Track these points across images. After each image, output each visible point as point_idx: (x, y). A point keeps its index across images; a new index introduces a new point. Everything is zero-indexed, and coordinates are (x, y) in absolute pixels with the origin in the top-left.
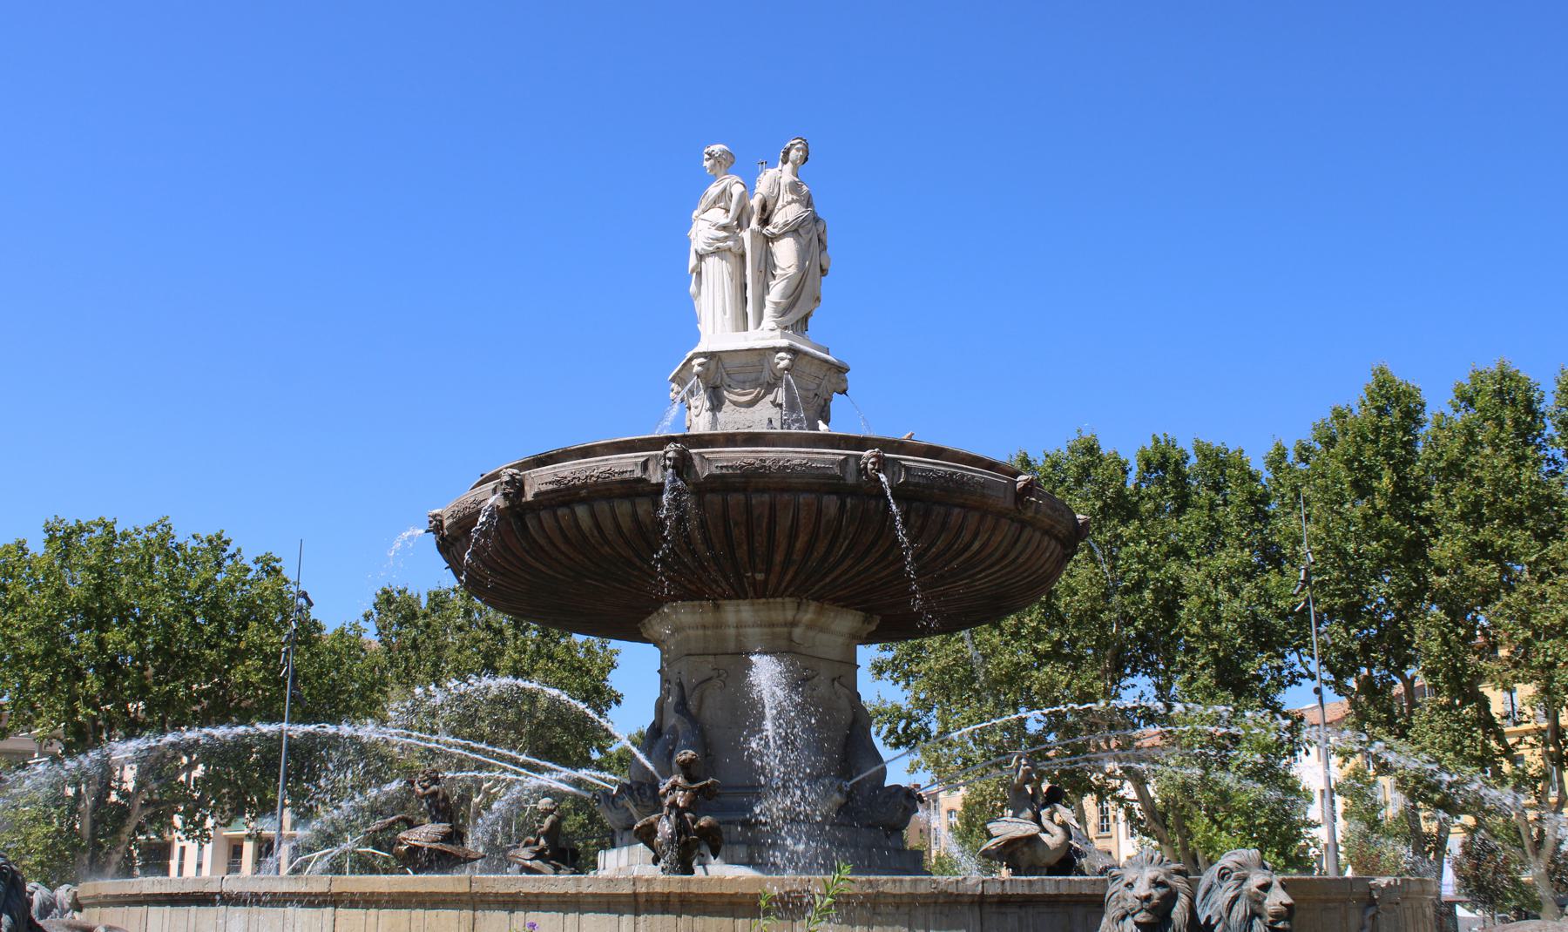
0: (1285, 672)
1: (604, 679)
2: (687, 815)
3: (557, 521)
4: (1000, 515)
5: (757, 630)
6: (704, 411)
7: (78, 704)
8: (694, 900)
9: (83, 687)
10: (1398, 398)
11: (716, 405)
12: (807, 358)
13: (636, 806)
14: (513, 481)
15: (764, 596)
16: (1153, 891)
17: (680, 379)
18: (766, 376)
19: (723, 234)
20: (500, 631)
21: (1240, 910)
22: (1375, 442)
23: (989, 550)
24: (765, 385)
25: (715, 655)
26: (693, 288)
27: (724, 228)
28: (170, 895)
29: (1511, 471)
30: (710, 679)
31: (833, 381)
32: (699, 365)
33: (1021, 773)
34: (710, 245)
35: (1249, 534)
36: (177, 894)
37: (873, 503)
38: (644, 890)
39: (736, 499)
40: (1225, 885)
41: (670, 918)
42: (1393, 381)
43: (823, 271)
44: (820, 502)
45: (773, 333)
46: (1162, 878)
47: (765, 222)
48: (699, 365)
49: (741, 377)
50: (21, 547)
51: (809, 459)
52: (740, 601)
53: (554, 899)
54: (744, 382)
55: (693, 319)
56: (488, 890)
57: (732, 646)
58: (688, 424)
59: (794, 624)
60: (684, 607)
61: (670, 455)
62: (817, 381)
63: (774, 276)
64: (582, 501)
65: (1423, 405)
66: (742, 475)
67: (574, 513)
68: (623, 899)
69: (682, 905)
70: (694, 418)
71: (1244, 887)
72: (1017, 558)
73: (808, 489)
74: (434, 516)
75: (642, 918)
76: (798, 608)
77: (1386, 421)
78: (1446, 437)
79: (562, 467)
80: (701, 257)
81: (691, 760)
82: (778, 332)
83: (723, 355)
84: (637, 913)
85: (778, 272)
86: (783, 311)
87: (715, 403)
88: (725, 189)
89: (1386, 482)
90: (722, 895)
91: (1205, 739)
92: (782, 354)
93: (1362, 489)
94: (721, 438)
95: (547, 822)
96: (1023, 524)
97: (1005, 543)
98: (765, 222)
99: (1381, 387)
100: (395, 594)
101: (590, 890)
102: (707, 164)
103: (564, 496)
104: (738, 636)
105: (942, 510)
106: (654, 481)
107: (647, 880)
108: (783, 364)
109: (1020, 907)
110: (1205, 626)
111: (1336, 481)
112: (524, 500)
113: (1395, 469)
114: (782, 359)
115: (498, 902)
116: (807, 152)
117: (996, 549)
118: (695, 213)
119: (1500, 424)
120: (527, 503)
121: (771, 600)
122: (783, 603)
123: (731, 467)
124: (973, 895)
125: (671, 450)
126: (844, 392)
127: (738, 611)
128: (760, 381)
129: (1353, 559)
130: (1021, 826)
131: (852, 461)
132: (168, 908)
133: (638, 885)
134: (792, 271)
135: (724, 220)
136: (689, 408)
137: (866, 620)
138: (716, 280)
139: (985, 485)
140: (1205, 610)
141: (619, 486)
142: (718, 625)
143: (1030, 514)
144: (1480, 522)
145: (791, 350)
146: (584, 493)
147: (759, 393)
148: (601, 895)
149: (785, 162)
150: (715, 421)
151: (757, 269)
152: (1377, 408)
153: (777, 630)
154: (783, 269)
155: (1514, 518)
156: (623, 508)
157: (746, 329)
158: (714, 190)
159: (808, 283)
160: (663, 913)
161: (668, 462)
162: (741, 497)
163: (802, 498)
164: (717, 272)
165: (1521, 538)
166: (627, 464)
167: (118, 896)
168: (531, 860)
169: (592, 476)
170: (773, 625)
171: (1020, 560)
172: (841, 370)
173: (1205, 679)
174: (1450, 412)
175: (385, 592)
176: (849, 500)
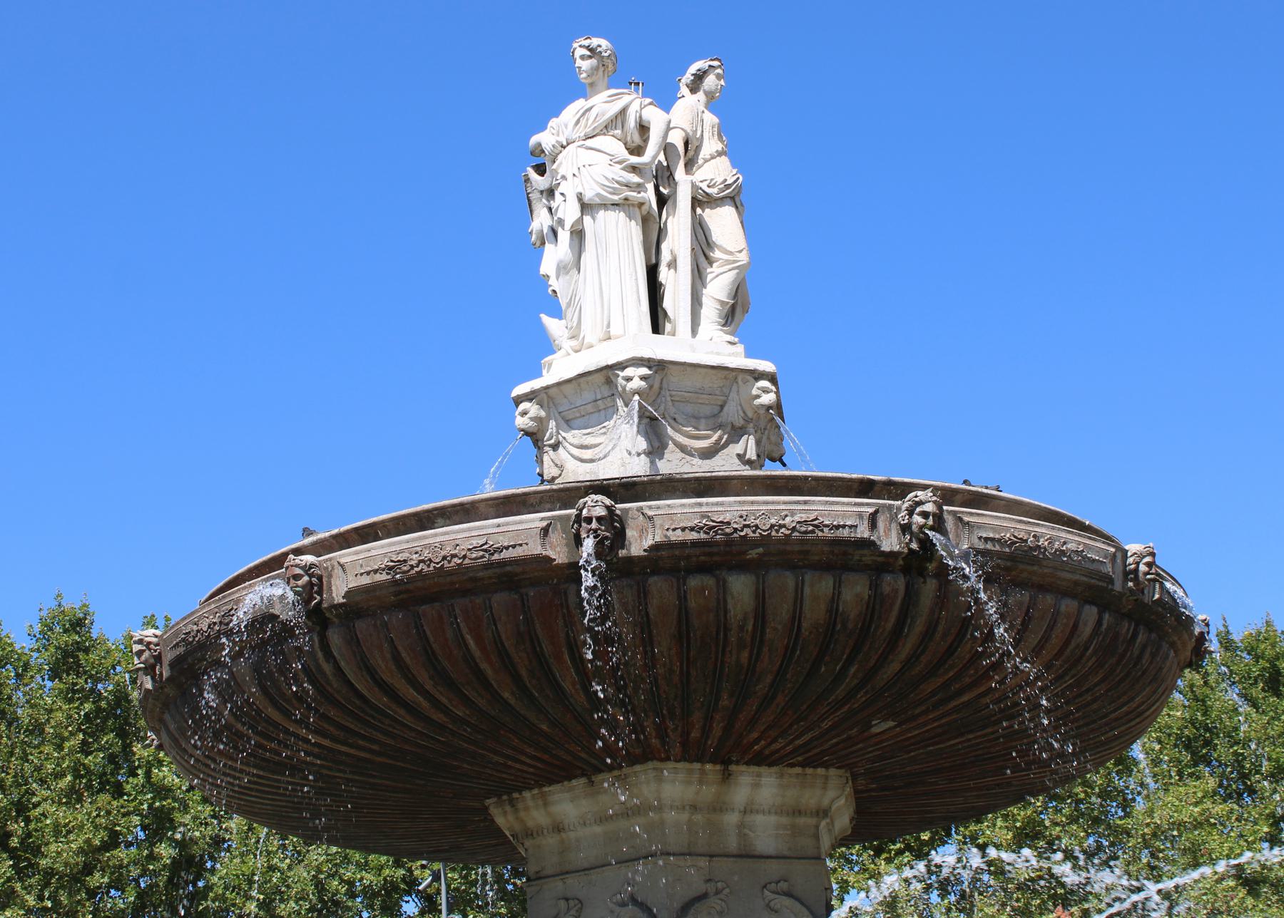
3: (683, 598)
5: (773, 819)
18: (732, 413)
24: (729, 428)
25: (712, 856)
30: (703, 897)
32: (643, 378)
44: (1079, 612)
45: (732, 349)
48: (643, 378)
49: (689, 408)
54: (697, 418)
57: (732, 844)
60: (676, 770)
64: (743, 566)
67: (723, 586)
76: (546, 804)
79: (717, 504)
87: (656, 444)
92: (764, 383)
102: (585, 65)
104: (741, 826)
112: (622, 553)
114: (766, 391)
120: (630, 560)
121: (809, 771)
122: (826, 778)
123: (999, 541)
127: (756, 786)
141: (826, 549)
146: (753, 553)
147: (720, 438)
153: (801, 821)
154: (731, 253)
156: (819, 587)
161: (918, 519)
162: (709, 581)
163: (1068, 605)
169: (781, 526)
170: (800, 812)
174: (112, 640)
176: (1107, 616)
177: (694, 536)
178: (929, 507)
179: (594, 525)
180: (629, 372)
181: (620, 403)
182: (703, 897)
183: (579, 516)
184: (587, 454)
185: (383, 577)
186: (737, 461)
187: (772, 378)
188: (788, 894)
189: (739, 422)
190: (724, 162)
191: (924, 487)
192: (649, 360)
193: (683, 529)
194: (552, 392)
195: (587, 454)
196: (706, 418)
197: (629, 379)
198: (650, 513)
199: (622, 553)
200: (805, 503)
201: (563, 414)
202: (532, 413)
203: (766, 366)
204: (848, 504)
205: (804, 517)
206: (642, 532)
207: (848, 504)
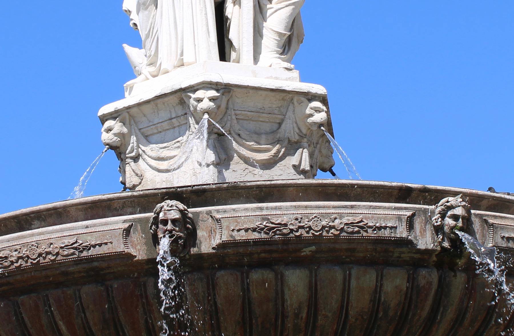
3: (246, 290)
24: (286, 142)
32: (212, 99)
48: (212, 99)
49: (252, 126)
54: (259, 134)
67: (281, 279)
79: (276, 208)
87: (223, 157)
120: (200, 256)
141: (370, 247)
146: (307, 251)
147: (279, 151)
161: (449, 222)
162: (268, 275)
169: (331, 227)
177: (256, 236)
178: (459, 211)
179: (170, 226)
180: (200, 94)
181: (192, 121)
183: (156, 218)
184: (163, 165)
186: (293, 171)
187: (324, 100)
189: (295, 138)
191: (455, 194)
192: (217, 84)
193: (247, 230)
194: (133, 111)
195: (163, 165)
196: (267, 133)
197: (199, 100)
198: (218, 216)
199: (194, 250)
200: (352, 207)
201: (142, 130)
202: (116, 130)
203: (318, 89)
204: (389, 208)
205: (351, 219)
206: (211, 232)
207: (389, 208)
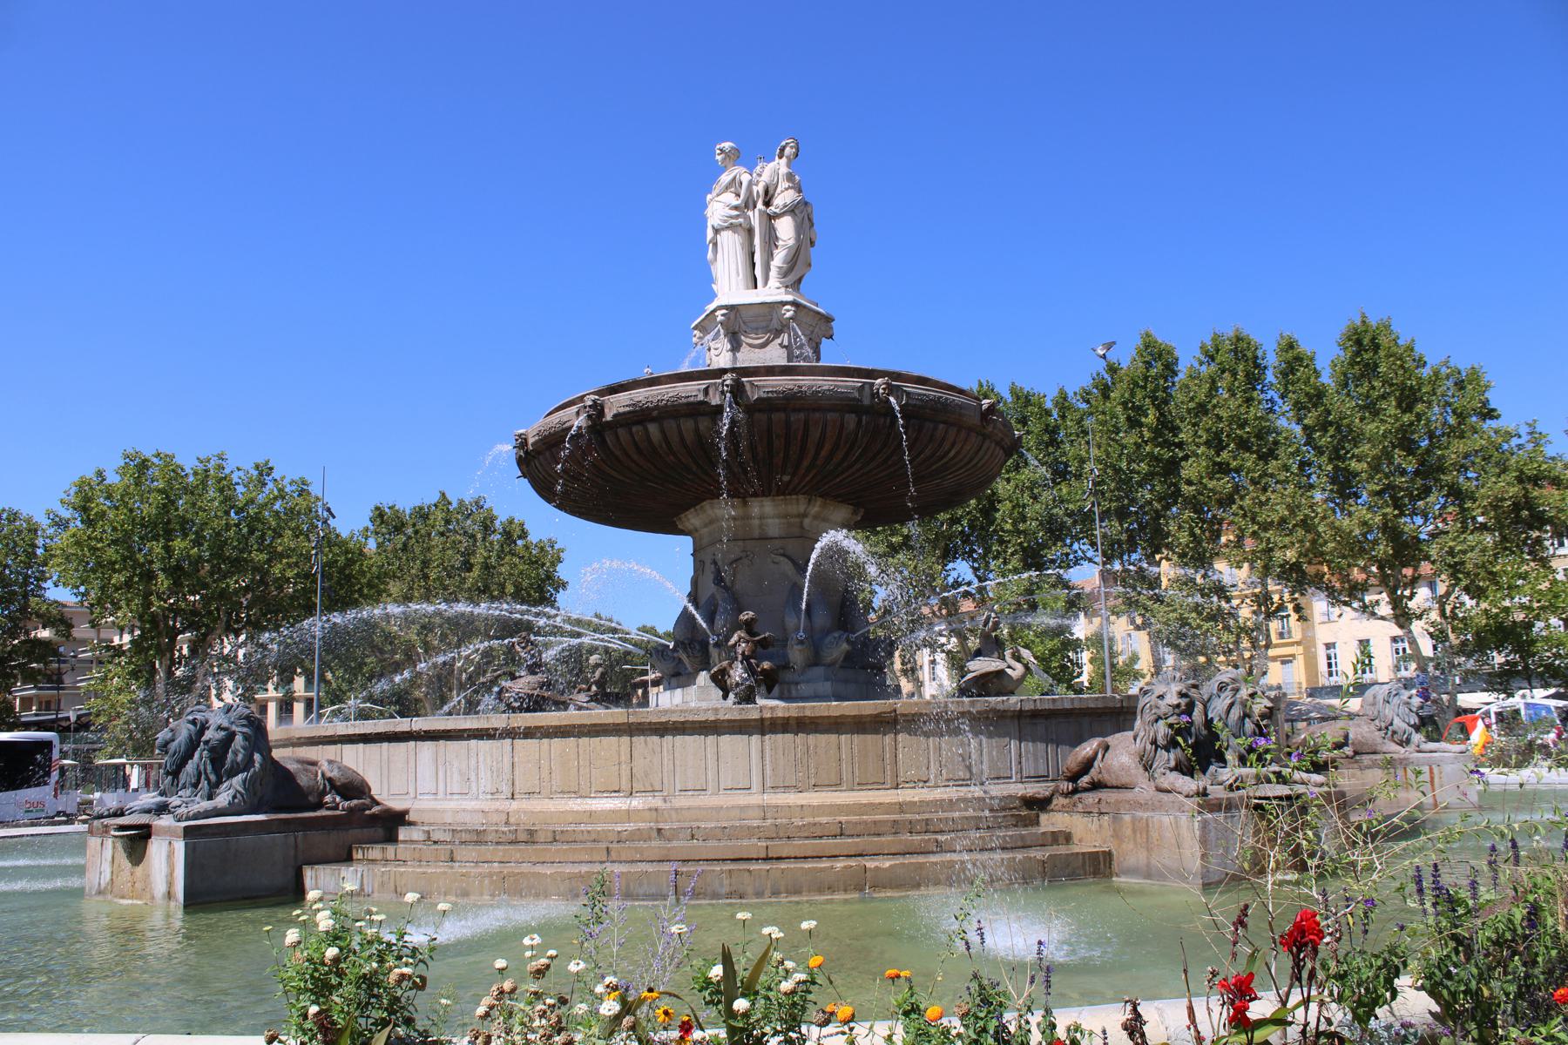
0: (1071, 557)
1: (555, 571)
2: (752, 661)
3: (632, 435)
4: (970, 429)
5: (777, 521)
6: (724, 351)
7: (153, 598)
8: (808, 721)
9: (155, 585)
10: (1160, 355)
11: (736, 347)
12: (805, 310)
13: (688, 657)
14: (595, 405)
15: (784, 494)
16: (1180, 700)
17: (703, 328)
18: (775, 324)
19: (736, 213)
20: (473, 536)
21: (1236, 713)
22: (1144, 387)
23: (960, 457)
26: (710, 255)
27: (736, 208)
28: (364, 735)
29: (1243, 410)
30: (740, 558)
31: (823, 328)
32: (722, 315)
33: (991, 624)
34: (725, 221)
35: (1044, 456)
36: (370, 734)
37: (882, 420)
38: (769, 715)
39: (778, 417)
40: (1223, 696)
41: (789, 736)
42: (1156, 342)
43: (812, 243)
46: (1184, 691)
47: (767, 204)
48: (722, 315)
50: (100, 474)
51: (836, 386)
52: (763, 499)
53: (697, 725)
54: (757, 329)
55: (710, 279)
56: (643, 720)
57: (756, 533)
58: (708, 362)
59: (805, 515)
61: (728, 382)
62: (811, 329)
63: (777, 247)
64: (653, 420)
65: (1177, 360)
66: (784, 398)
67: (646, 430)
68: (752, 723)
69: (798, 726)
70: (714, 358)
71: (1238, 696)
72: (978, 463)
73: (833, 409)
74: (520, 435)
75: (767, 737)
77: (1153, 372)
78: (1196, 385)
80: (717, 231)
81: (752, 619)
82: (783, 290)
83: (740, 308)
84: (763, 734)
85: (780, 243)
86: (785, 273)
88: (735, 178)
89: (1151, 418)
90: (829, 717)
91: (1014, 607)
93: (1134, 423)
94: (762, 370)
95: (597, 674)
96: (985, 437)
97: (972, 452)
98: (767, 204)
99: (1147, 347)
100: (387, 510)
101: (727, 717)
102: (719, 158)
103: (639, 416)
104: (761, 526)
105: (931, 425)
106: (713, 403)
107: (771, 708)
108: (788, 315)
109: (1046, 719)
110: (1014, 524)
111: (1114, 416)
113: (1158, 408)
114: (788, 311)
115: (651, 729)
116: (798, 150)
117: (965, 456)
118: (709, 197)
119: (1234, 374)
120: (607, 422)
121: (788, 497)
122: (797, 500)
124: (1015, 711)
125: (728, 379)
126: (831, 337)
127: (762, 506)
128: (771, 327)
129: (1126, 474)
130: (993, 664)
131: (867, 387)
132: (361, 745)
133: (764, 711)
134: (791, 242)
135: (736, 202)
136: (709, 350)
137: (855, 513)
138: (730, 248)
139: (961, 406)
140: (1016, 512)
142: (747, 517)
143: (990, 429)
144: (1220, 448)
145: (794, 303)
146: (655, 413)
148: (735, 721)
149: (780, 157)
150: (735, 359)
151: (763, 241)
152: (1144, 362)
155: (1243, 445)
156: (687, 425)
157: (756, 287)
158: (725, 178)
159: (802, 252)
160: (783, 733)
161: (725, 388)
162: (782, 415)
163: (830, 416)
164: (730, 243)
165: (1250, 460)
166: (692, 390)
167: (313, 737)
168: (587, 702)
171: (979, 465)
172: (828, 319)
173: (1015, 562)
175: (377, 508)
176: (864, 417)
177: (628, 409)
182: (740, 558)
185: (537, 438)
188: (784, 555)
190: (791, 192)
